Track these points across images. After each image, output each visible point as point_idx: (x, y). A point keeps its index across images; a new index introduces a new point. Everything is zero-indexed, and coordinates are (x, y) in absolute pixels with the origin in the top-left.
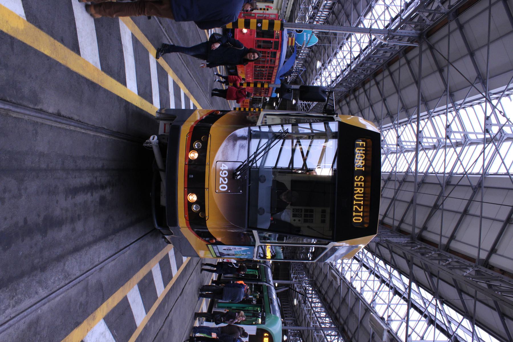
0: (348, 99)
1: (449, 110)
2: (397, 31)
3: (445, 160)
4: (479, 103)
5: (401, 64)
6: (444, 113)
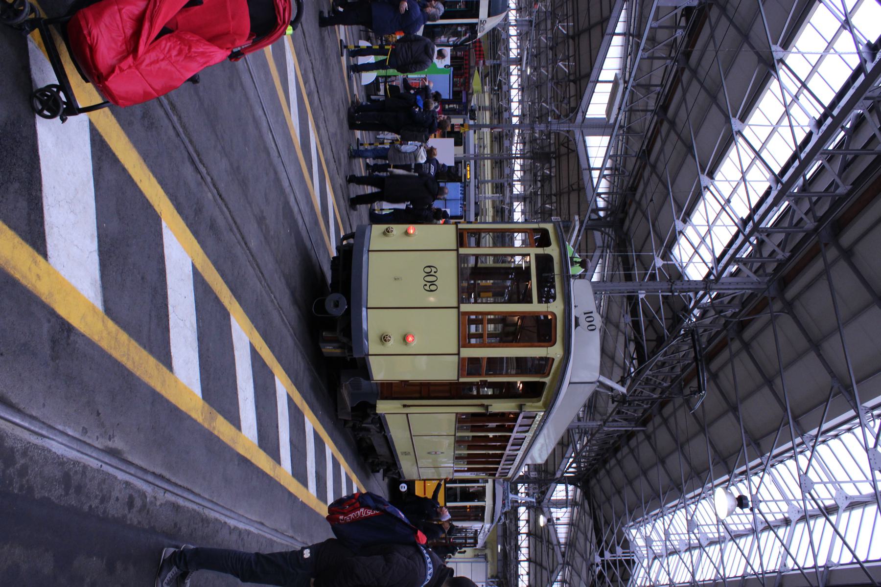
0: (619, 455)
1: (798, 450)
2: (721, 281)
3: (811, 542)
4: (849, 430)
5: (639, 440)
6: (791, 457)
